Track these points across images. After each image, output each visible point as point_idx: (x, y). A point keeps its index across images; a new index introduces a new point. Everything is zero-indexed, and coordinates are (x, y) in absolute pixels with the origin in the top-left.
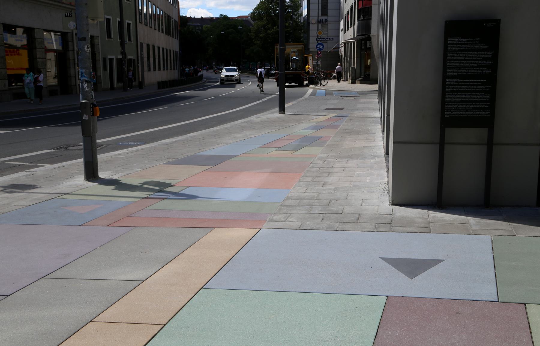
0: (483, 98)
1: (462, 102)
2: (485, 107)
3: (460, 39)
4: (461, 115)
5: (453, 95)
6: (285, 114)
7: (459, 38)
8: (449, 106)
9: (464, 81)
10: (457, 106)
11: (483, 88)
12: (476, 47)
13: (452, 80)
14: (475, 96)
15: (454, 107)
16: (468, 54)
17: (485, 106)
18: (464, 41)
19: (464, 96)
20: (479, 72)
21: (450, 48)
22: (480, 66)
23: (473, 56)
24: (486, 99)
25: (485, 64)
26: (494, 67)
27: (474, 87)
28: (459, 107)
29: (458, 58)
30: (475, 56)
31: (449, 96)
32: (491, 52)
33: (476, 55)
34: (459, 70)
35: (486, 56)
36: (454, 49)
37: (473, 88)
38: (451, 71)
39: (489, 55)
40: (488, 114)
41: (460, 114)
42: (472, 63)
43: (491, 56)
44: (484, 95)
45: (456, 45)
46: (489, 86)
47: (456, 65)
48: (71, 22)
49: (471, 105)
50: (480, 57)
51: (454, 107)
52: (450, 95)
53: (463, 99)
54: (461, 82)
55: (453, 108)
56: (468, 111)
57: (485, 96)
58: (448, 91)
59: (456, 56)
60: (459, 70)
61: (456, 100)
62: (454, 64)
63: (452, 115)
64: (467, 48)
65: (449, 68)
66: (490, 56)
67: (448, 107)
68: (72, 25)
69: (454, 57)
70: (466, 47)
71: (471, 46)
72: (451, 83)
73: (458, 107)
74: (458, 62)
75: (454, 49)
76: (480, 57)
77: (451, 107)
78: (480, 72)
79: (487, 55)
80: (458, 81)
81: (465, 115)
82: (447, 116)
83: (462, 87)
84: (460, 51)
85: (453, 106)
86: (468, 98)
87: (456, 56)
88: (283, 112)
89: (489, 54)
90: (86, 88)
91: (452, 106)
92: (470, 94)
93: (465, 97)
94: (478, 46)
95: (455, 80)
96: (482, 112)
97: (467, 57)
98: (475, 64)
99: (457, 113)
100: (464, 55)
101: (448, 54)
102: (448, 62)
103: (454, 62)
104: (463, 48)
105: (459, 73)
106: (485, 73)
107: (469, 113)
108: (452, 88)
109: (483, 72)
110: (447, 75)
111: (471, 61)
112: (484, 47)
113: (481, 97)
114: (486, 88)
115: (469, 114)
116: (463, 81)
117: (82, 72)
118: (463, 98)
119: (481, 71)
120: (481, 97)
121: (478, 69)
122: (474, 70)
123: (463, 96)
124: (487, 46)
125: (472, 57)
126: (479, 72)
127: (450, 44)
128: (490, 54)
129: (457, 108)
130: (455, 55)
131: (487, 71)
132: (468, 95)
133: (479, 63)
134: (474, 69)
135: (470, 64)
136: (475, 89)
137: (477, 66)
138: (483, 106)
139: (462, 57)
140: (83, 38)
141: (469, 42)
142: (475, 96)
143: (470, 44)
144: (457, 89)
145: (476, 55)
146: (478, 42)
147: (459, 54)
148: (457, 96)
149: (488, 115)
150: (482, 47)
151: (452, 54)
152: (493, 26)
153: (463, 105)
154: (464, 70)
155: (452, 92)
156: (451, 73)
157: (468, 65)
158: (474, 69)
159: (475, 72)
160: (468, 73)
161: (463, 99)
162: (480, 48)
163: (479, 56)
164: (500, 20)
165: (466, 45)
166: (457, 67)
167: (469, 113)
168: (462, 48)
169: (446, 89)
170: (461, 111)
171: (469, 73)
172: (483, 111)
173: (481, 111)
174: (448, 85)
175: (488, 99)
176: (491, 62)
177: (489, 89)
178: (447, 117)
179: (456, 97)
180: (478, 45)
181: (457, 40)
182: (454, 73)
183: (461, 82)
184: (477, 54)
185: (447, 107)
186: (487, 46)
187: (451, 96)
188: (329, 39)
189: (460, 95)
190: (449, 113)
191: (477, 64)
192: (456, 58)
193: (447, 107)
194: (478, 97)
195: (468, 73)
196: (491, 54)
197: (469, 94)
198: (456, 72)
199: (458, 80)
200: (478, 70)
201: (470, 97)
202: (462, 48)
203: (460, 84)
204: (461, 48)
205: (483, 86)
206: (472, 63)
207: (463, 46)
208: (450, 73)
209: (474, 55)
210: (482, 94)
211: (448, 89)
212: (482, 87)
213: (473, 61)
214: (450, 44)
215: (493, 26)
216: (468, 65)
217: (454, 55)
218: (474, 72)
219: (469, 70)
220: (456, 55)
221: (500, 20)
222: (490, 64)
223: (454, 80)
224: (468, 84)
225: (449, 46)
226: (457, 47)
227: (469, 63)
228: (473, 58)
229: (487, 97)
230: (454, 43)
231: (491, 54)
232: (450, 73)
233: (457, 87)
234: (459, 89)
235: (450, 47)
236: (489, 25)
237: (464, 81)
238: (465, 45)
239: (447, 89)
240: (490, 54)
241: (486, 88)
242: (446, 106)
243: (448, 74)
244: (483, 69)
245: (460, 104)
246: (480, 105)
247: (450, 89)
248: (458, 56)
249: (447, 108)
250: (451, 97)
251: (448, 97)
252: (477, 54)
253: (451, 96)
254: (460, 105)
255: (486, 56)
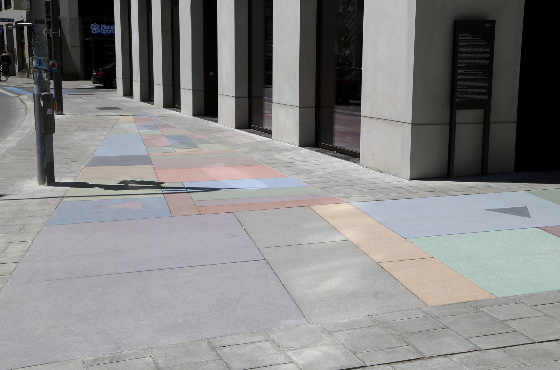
1: (469, 88)
6: (63, 115)
22: (481, 59)
26: (491, 59)
40: (487, 97)
48: (24, 1)
54: (468, 71)
65: (459, 59)
68: (26, 5)
71: (475, 42)
84: (468, 45)
88: (61, 112)
89: (488, 49)
90: (45, 78)
114: (486, 76)
117: (39, 60)
127: (460, 40)
137: (479, 58)
140: (41, 20)
143: (475, 40)
146: (480, 38)
155: (462, 80)
164: (495, 21)
166: (465, 59)
169: (458, 78)
174: (459, 74)
183: (468, 71)
188: (8, 20)
214: (460, 40)
221: (495, 21)
224: (473, 73)
236: (488, 25)
238: (471, 41)
241: (486, 76)
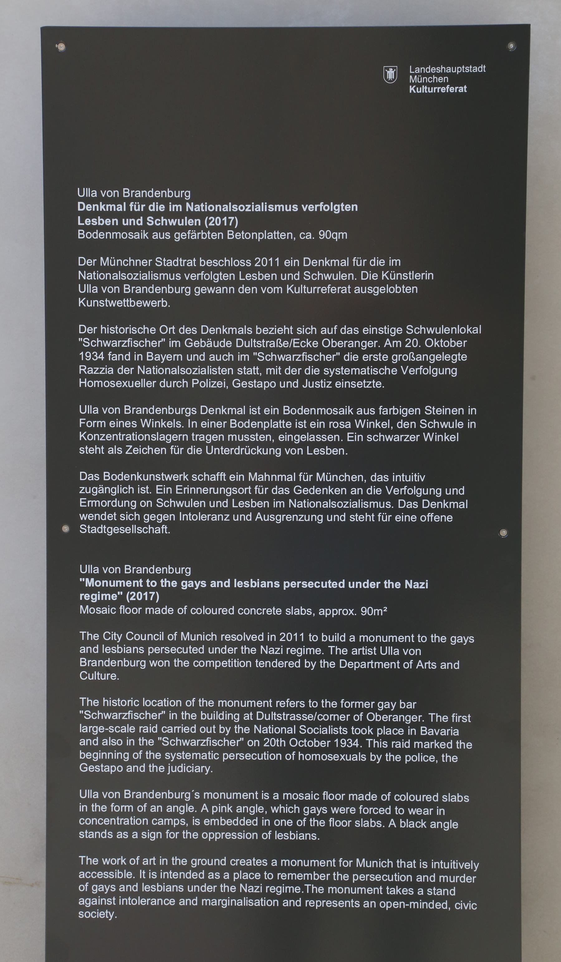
0: (406, 744)
2: (434, 825)
3: (182, 201)
4: (226, 903)
5: (141, 709)
7: (169, 193)
8: (109, 814)
9: (239, 584)
10: (188, 817)
11: (403, 658)
12: (324, 283)
13: (134, 577)
14: (336, 724)
15: (162, 829)
16: (261, 344)
17: (428, 819)
18: (216, 221)
19: (243, 723)
20: (361, 511)
21: (93, 283)
23: (304, 364)
24: (437, 752)
25: (413, 438)
27: (324, 646)
28: (202, 829)
29: (170, 378)
30: (322, 365)
31: (106, 723)
32: (459, 330)
33: (329, 358)
34: (189, 490)
35: (415, 364)
36: (135, 297)
37: (318, 651)
38: (120, 497)
39: (446, 357)
41: (217, 895)
42: (301, 425)
43: (459, 364)
44: (414, 718)
45: (144, 263)
46: (456, 640)
47: (154, 437)
49: (302, 804)
50: (364, 371)
51: (162, 822)
52: (116, 716)
53: (231, 756)
55: (153, 836)
56: (285, 862)
57: (424, 731)
58: (97, 676)
59: (150, 356)
60: (189, 490)
61: (177, 762)
62: (140, 430)
63: (142, 902)
64: (245, 290)
66: (449, 364)
67: (107, 821)
69: (132, 364)
70: (236, 283)
71: (283, 270)
72: (121, 600)
73: (192, 829)
74: (169, 410)
75: (135, 297)
76: (364, 371)
77: (133, 821)
78: (375, 511)
79: (420, 358)
80: (185, 585)
81: (253, 896)
82: (103, 908)
83: (221, 644)
85: (148, 815)
86: (279, 742)
87: (150, 356)
91: (136, 814)
92: (293, 704)
93: (253, 736)
94: (342, 277)
95: (157, 577)
96: (404, 871)
97: (254, 370)
98: (327, 431)
99: (186, 882)
100: (224, 351)
101: (86, 342)
102: (89, 409)
103: (140, 411)
104: (210, 284)
105: (190, 517)
106: (413, 518)
107: (294, 883)
108: (129, 650)
109: (395, 511)
110: (84, 529)
111: (287, 410)
112: (392, 283)
113: (389, 732)
115: (297, 890)
116: (227, 584)
118: (232, 743)
119: (383, 497)
120: (389, 732)
121: (349, 485)
122: (317, 491)
123: (227, 723)
124: (418, 276)
125: (293, 371)
126: (361, 511)
128: (454, 351)
129: (186, 834)
130: (143, 351)
131: (432, 498)
132: (274, 716)
133: (353, 429)
134: (186, 644)
135: (281, 438)
136: (332, 665)
138: (415, 818)
139: (203, 371)
141: (259, 236)
142: (336, 724)
144: (177, 662)
145: (331, 351)
146: (337, 236)
147: (182, 338)
148: (178, 722)
149: (460, 906)
150: (380, 283)
151: (116, 344)
152: (463, 89)
153: (235, 803)
154: (228, 484)
156: (119, 511)
157: (265, 445)
158: (314, 483)
159: (326, 505)
160: (264, 511)
161: (231, 756)
162: (358, 290)
163: (361, 364)
165: (242, 263)
167: (294, 883)
168: (201, 283)
169: (83, 662)
170: (222, 862)
171: (279, 519)
172: (411, 865)
173: (400, 863)
175: (454, 759)
176: (464, 418)
177: (456, 665)
178: (101, 915)
179: (170, 730)
180: (345, 263)
181: (156, 215)
182: (149, 518)
184: (340, 344)
185: (101, 828)
186: (418, 276)
187: (132, 722)
189: (208, 710)
190: (117, 882)
191: (343, 433)
192: (158, 378)
193: (101, 828)
194: (362, 739)
195: (264, 511)
196: (459, 344)
197: (281, 704)
198: (161, 503)
199: (180, 578)
200: (355, 491)
201: (291, 731)
202: (201, 283)
203: (204, 611)
204: (193, 284)
205: (401, 639)
206: (301, 425)
207: (207, 269)
208: (110, 510)
209: (310, 358)
210: (398, 711)
211: (95, 663)
212: (395, 645)
213: (305, 411)
215: (463, 89)
216: (265, 445)
217: (132, 350)
218: (317, 511)
219: (269, 484)
220: (155, 351)
222: (453, 438)
223: (144, 577)
225: (89, 269)
226: (156, 277)
227: (276, 425)
228: (302, 378)
229: (440, 739)
230: (131, 236)
231: (459, 344)
232: (110, 510)
233: (178, 643)
234: (191, 657)
235: (91, 276)
237: (239, 584)
239: (89, 656)
240: (454, 351)
242: (90, 814)
243: (96, 523)
244: (399, 485)
245: (212, 795)
246: (382, 811)
247: (112, 663)
248: (169, 357)
249: (92, 835)
250: (124, 729)
251: (102, 736)
252: (340, 344)
253: (121, 723)
254: (211, 803)
255: (415, 364)
